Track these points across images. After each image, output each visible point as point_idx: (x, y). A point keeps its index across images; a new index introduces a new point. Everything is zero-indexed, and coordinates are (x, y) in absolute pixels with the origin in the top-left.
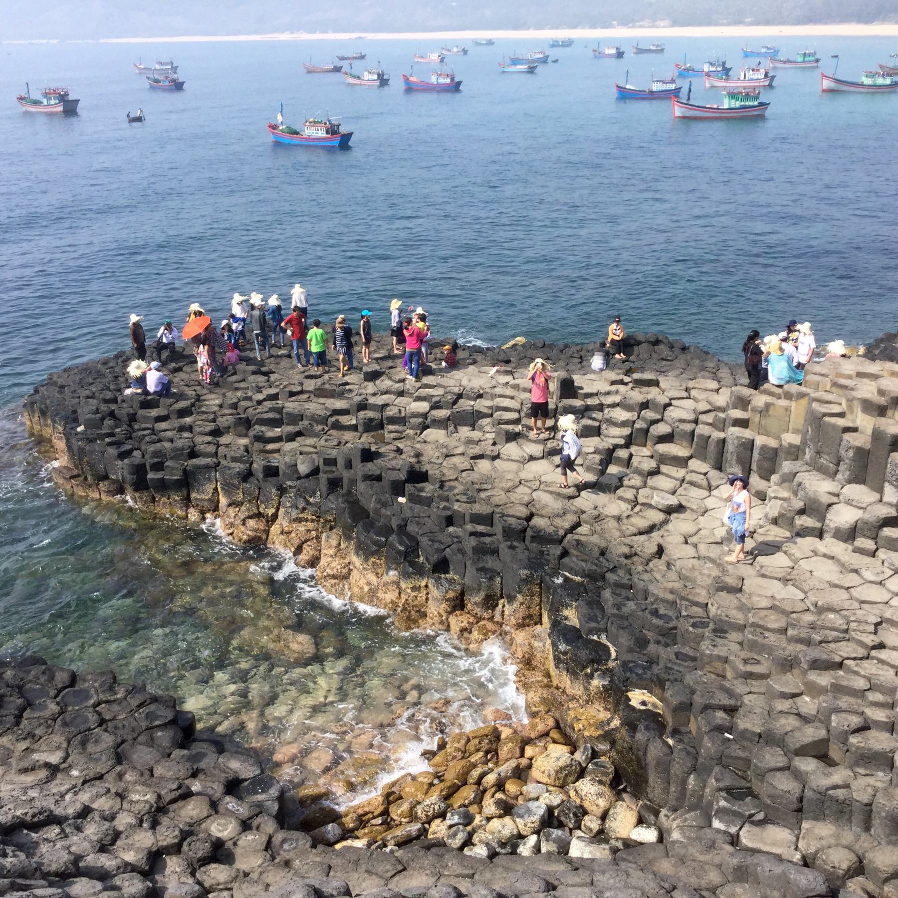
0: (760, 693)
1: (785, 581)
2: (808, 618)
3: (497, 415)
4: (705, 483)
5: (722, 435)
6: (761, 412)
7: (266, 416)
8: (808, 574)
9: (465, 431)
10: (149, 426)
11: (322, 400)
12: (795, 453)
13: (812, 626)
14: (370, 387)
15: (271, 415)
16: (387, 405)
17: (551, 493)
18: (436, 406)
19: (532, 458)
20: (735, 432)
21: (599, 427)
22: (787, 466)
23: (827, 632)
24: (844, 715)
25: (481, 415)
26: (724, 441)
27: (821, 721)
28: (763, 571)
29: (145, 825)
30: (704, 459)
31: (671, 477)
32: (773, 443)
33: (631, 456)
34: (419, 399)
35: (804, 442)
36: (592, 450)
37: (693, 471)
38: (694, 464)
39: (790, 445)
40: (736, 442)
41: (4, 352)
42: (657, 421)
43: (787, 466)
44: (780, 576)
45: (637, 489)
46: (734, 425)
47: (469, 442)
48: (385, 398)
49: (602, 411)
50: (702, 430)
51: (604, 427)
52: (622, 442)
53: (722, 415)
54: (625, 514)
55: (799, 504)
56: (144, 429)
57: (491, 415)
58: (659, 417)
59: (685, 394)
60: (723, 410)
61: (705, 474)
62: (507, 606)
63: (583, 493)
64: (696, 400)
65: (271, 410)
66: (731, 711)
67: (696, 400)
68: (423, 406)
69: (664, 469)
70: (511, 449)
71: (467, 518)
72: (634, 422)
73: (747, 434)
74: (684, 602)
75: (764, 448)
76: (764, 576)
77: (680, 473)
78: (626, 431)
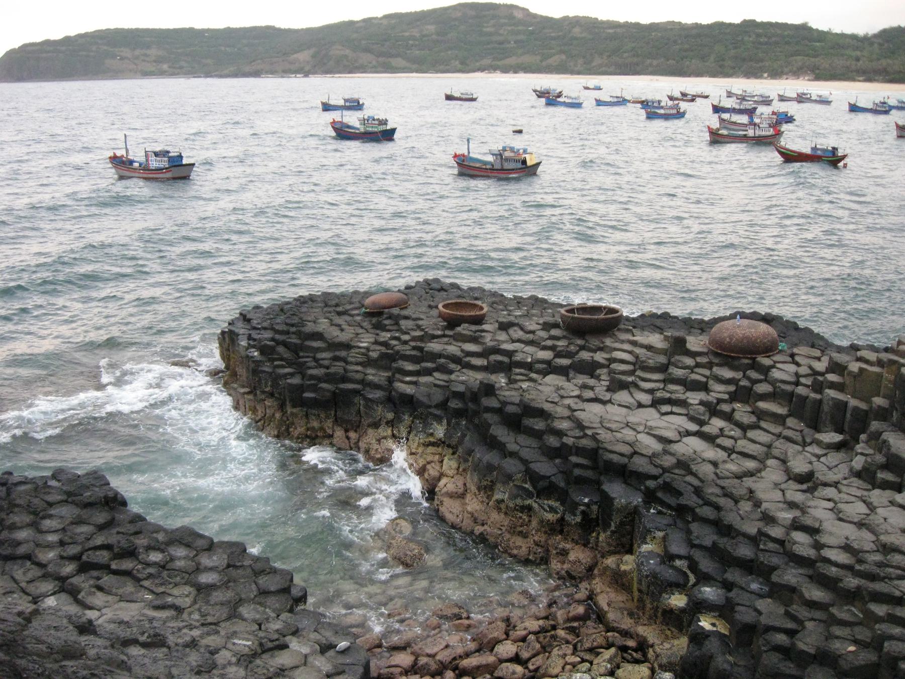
0: (820, 621)
1: (860, 525)
2: (878, 557)
3: (614, 366)
4: (800, 439)
5: (818, 397)
6: (855, 377)
7: (408, 353)
8: (882, 520)
9: (582, 379)
10: (311, 355)
11: (460, 344)
12: (883, 415)
13: (880, 565)
14: (502, 336)
15: (413, 353)
16: (516, 351)
17: (654, 436)
18: (558, 355)
19: (640, 405)
20: (832, 393)
21: (707, 383)
22: (875, 425)
23: (891, 570)
24: (895, 642)
25: (600, 366)
26: (821, 401)
27: (875, 648)
28: (841, 515)
29: (431, 431)
30: (801, 418)
31: (768, 432)
32: (863, 406)
33: (734, 410)
34: (545, 348)
35: (892, 406)
36: (697, 402)
37: (789, 428)
38: (790, 422)
39: (879, 406)
40: (831, 403)
41: (7, 318)
42: (760, 381)
43: (875, 425)
44: (856, 520)
45: (736, 440)
46: (830, 388)
47: (584, 387)
48: (517, 346)
49: (711, 369)
50: (800, 390)
51: (711, 382)
52: (726, 397)
53: (820, 378)
54: (721, 460)
55: (880, 459)
56: (308, 357)
57: (608, 366)
58: (762, 377)
59: (790, 359)
60: (822, 374)
61: (801, 431)
62: (602, 534)
63: (685, 440)
64: (798, 364)
65: (414, 348)
66: (791, 633)
67: (798, 364)
68: (546, 355)
69: (763, 424)
70: (623, 396)
71: (574, 451)
72: (739, 380)
73: (840, 396)
74: (762, 538)
75: (856, 409)
76: (840, 519)
77: (777, 429)
78: (732, 388)
